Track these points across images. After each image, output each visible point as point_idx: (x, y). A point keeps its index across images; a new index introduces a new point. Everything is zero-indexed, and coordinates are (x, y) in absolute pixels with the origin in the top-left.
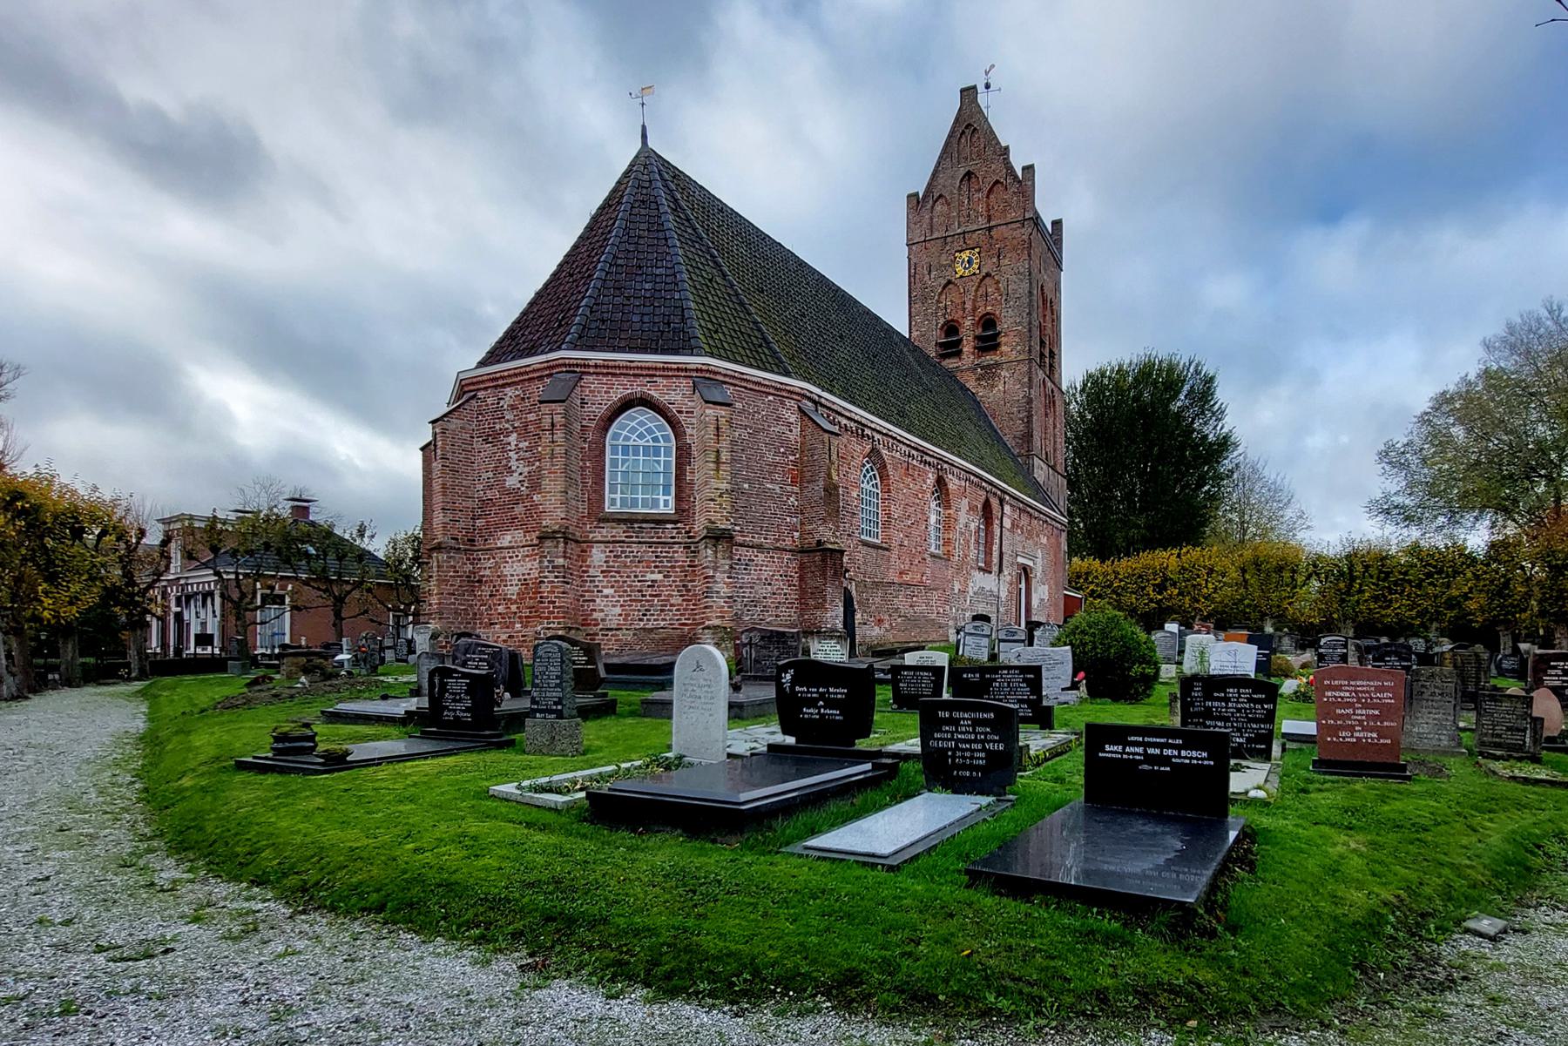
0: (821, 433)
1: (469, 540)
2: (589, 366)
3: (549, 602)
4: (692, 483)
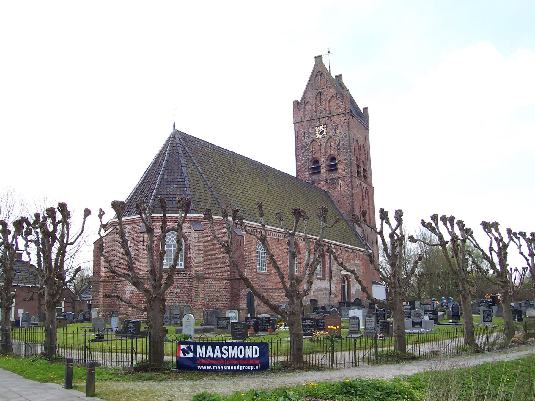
0: (237, 236)
1: (113, 278)
2: (155, 218)
3: (142, 300)
4: (190, 257)
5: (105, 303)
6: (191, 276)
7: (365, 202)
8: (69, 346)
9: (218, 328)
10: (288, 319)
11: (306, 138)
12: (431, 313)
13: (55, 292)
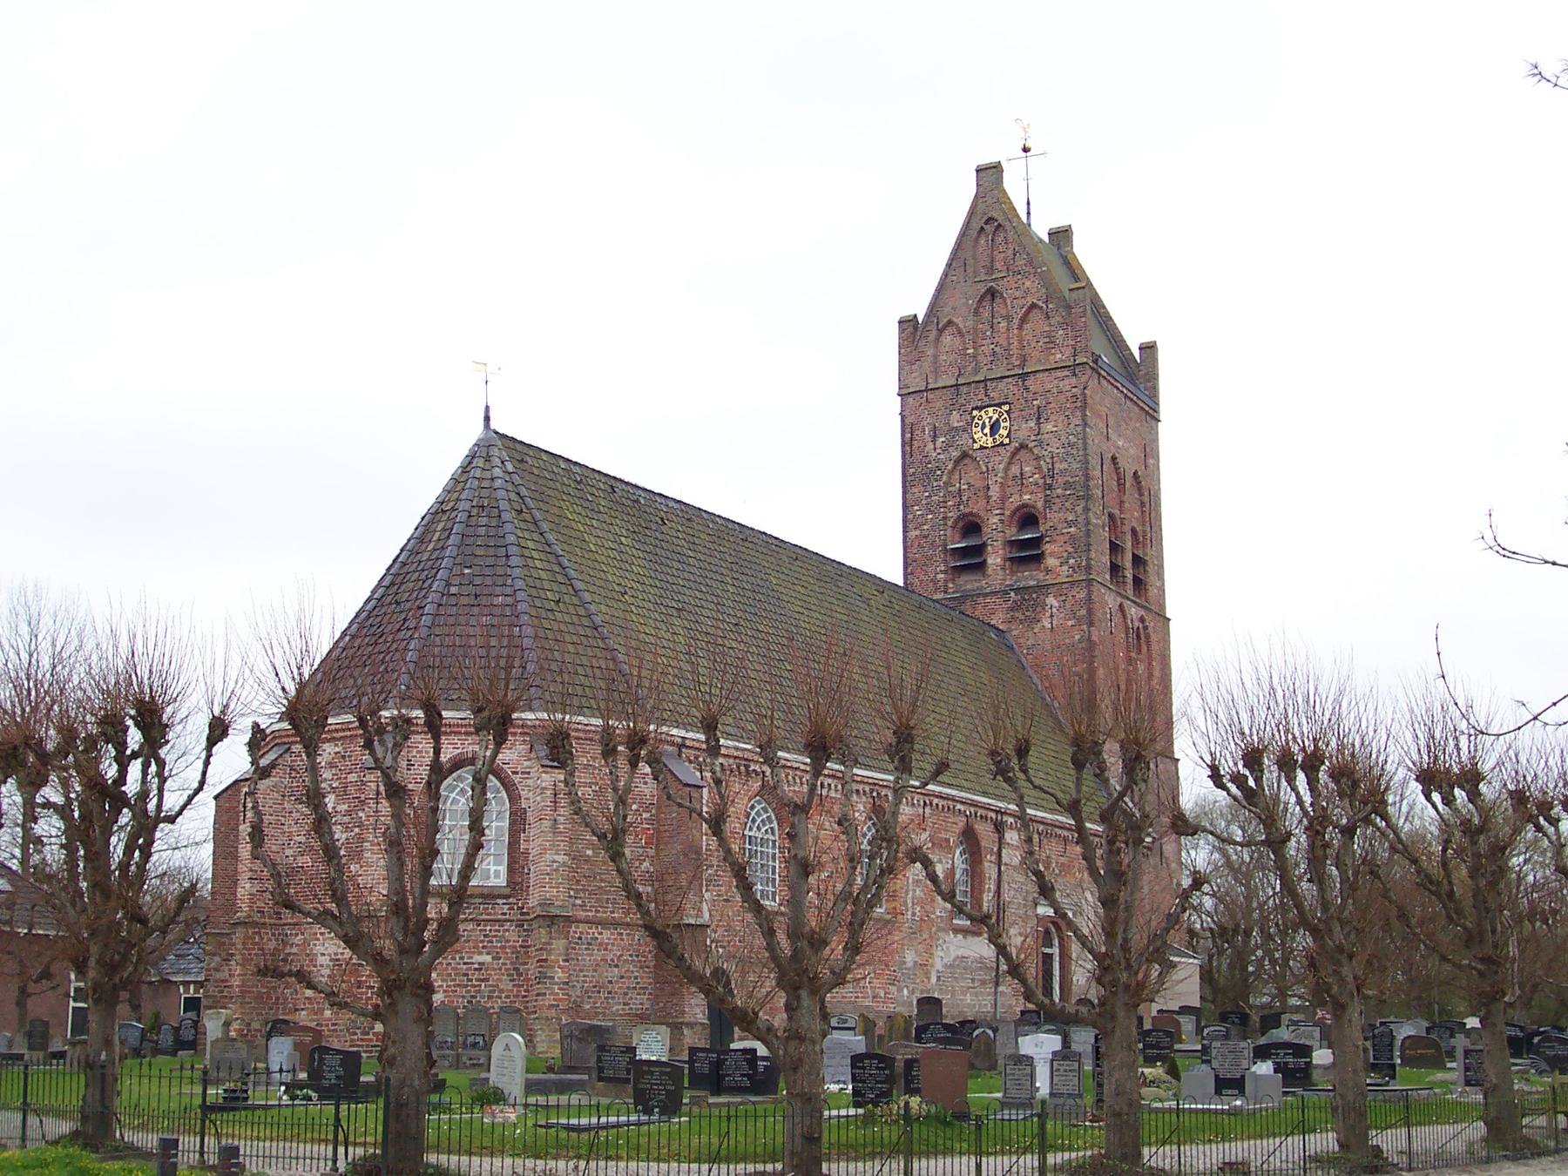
0: (680, 787)
5: (249, 992)
6: (528, 914)
7: (1136, 669)
8: (156, 1112)
9: (600, 1079)
10: (781, 1052)
11: (938, 444)
12: (1290, 1054)
13: (116, 957)
